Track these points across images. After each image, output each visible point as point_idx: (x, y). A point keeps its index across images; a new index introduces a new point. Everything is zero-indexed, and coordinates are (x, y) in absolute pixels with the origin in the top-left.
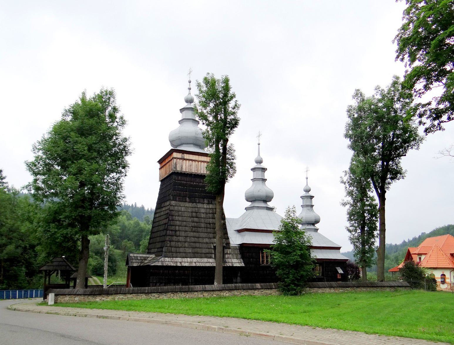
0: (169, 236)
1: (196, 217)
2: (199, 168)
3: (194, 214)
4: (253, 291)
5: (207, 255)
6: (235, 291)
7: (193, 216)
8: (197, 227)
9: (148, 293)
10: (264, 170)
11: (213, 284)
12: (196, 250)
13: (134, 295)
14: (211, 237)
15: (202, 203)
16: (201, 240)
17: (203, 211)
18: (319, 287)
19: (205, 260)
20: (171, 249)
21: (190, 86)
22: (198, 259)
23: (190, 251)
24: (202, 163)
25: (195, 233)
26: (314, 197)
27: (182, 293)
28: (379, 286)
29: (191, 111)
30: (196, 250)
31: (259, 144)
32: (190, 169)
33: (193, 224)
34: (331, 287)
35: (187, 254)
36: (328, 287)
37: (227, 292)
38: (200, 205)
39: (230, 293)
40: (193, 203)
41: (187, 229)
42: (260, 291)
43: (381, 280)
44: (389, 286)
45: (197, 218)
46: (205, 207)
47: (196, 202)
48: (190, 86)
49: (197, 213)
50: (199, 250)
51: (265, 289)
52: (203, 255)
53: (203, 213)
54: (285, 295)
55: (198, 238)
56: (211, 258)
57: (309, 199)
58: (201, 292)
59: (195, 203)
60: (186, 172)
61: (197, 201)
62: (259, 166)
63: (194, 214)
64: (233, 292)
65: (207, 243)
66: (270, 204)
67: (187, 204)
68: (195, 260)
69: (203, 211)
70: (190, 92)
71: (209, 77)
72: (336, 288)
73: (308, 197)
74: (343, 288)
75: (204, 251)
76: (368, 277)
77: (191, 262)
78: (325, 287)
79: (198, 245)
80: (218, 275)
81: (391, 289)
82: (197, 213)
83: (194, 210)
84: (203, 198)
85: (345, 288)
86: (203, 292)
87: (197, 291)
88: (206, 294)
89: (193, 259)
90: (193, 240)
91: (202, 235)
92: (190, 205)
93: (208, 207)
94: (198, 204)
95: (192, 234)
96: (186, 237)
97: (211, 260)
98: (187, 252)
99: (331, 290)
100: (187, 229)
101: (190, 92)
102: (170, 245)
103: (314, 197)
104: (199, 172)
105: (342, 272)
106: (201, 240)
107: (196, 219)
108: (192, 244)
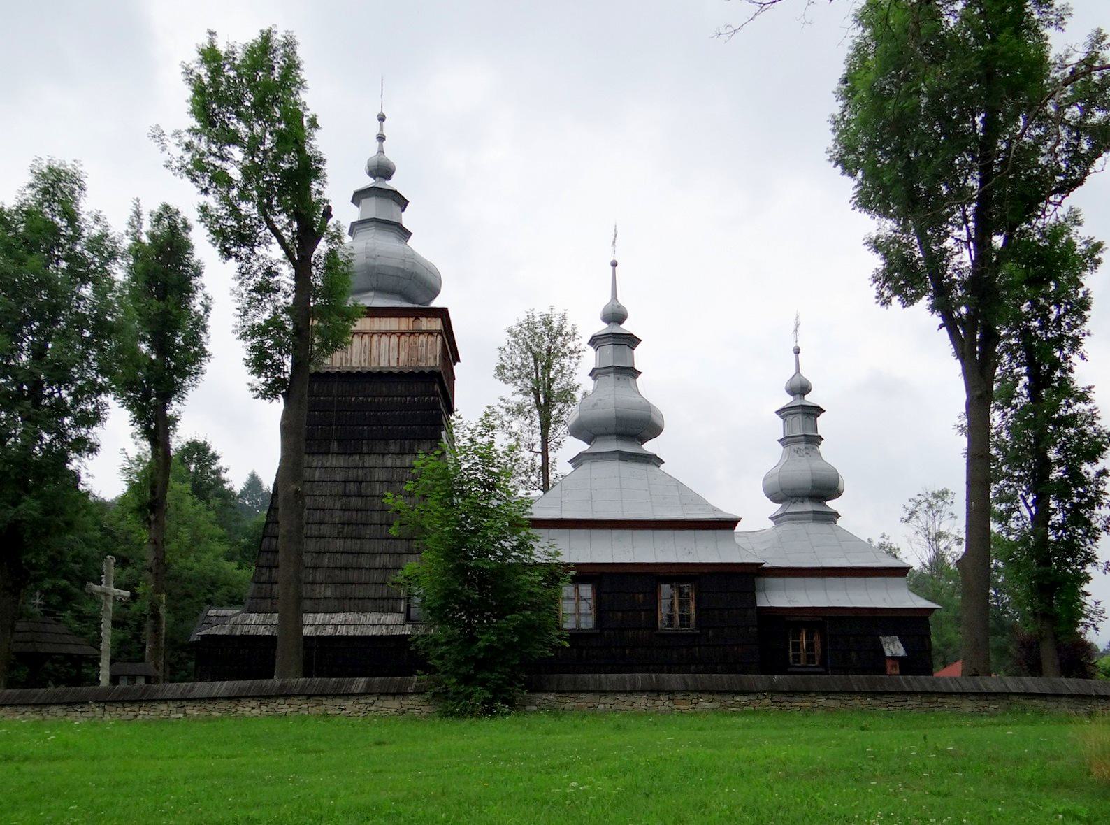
0: (268, 552)
1: (359, 496)
2: (375, 352)
3: (352, 488)
4: (339, 701)
5: (385, 604)
6: (278, 701)
7: (347, 491)
8: (357, 524)
9: (41, 705)
10: (632, 341)
11: (273, 678)
12: (347, 590)
13: (8, 708)
14: (399, 550)
15: (379, 454)
16: (364, 561)
17: (379, 475)
18: (602, 692)
19: (373, 618)
20: (268, 590)
21: (381, 129)
22: (350, 617)
23: (329, 593)
24: (385, 339)
25: (349, 541)
26: (824, 411)
27: (126, 704)
28: (917, 693)
29: (374, 198)
30: (347, 590)
31: (614, 264)
32: (347, 359)
33: (346, 516)
34: (656, 691)
35: (316, 601)
36: (643, 692)
37: (254, 703)
38: (371, 461)
39: (264, 708)
40: (351, 455)
41: (325, 529)
42: (363, 701)
43: (973, 672)
44: (975, 694)
45: (360, 499)
46: (389, 462)
47: (361, 453)
48: (381, 129)
49: (361, 482)
50: (359, 591)
51: (382, 694)
52: (370, 604)
53: (382, 482)
54: (447, 714)
55: (358, 553)
56: (393, 610)
57: (800, 416)
58: (179, 703)
59: (356, 454)
60: (332, 368)
61: (365, 450)
62: (616, 329)
63: (352, 488)
64: (273, 705)
65: (385, 569)
66: (649, 447)
67: (332, 461)
68: (338, 618)
69: (379, 475)
70: (381, 146)
71: (866, 240)
72: (679, 697)
73: (608, 370)
74: (716, 697)
75: (371, 593)
76: (54, 604)
77: (324, 625)
78: (631, 692)
79: (353, 575)
80: (286, 657)
81: (981, 703)
82: (361, 482)
83: (352, 474)
84: (386, 439)
85: (728, 697)
86: (184, 703)
87: (165, 701)
88: (192, 711)
89: (333, 615)
90: (342, 560)
91: (369, 546)
92: (341, 461)
93: (398, 463)
94: (366, 457)
95: (340, 544)
96: (319, 553)
97: (389, 618)
98: (318, 596)
99: (658, 703)
100: (325, 529)
101: (381, 146)
102: (270, 577)
103: (824, 411)
104: (375, 365)
105: (901, 652)
106: (364, 561)
107: (355, 502)
108: (337, 572)
